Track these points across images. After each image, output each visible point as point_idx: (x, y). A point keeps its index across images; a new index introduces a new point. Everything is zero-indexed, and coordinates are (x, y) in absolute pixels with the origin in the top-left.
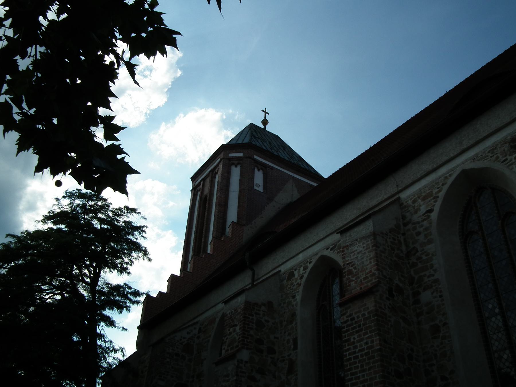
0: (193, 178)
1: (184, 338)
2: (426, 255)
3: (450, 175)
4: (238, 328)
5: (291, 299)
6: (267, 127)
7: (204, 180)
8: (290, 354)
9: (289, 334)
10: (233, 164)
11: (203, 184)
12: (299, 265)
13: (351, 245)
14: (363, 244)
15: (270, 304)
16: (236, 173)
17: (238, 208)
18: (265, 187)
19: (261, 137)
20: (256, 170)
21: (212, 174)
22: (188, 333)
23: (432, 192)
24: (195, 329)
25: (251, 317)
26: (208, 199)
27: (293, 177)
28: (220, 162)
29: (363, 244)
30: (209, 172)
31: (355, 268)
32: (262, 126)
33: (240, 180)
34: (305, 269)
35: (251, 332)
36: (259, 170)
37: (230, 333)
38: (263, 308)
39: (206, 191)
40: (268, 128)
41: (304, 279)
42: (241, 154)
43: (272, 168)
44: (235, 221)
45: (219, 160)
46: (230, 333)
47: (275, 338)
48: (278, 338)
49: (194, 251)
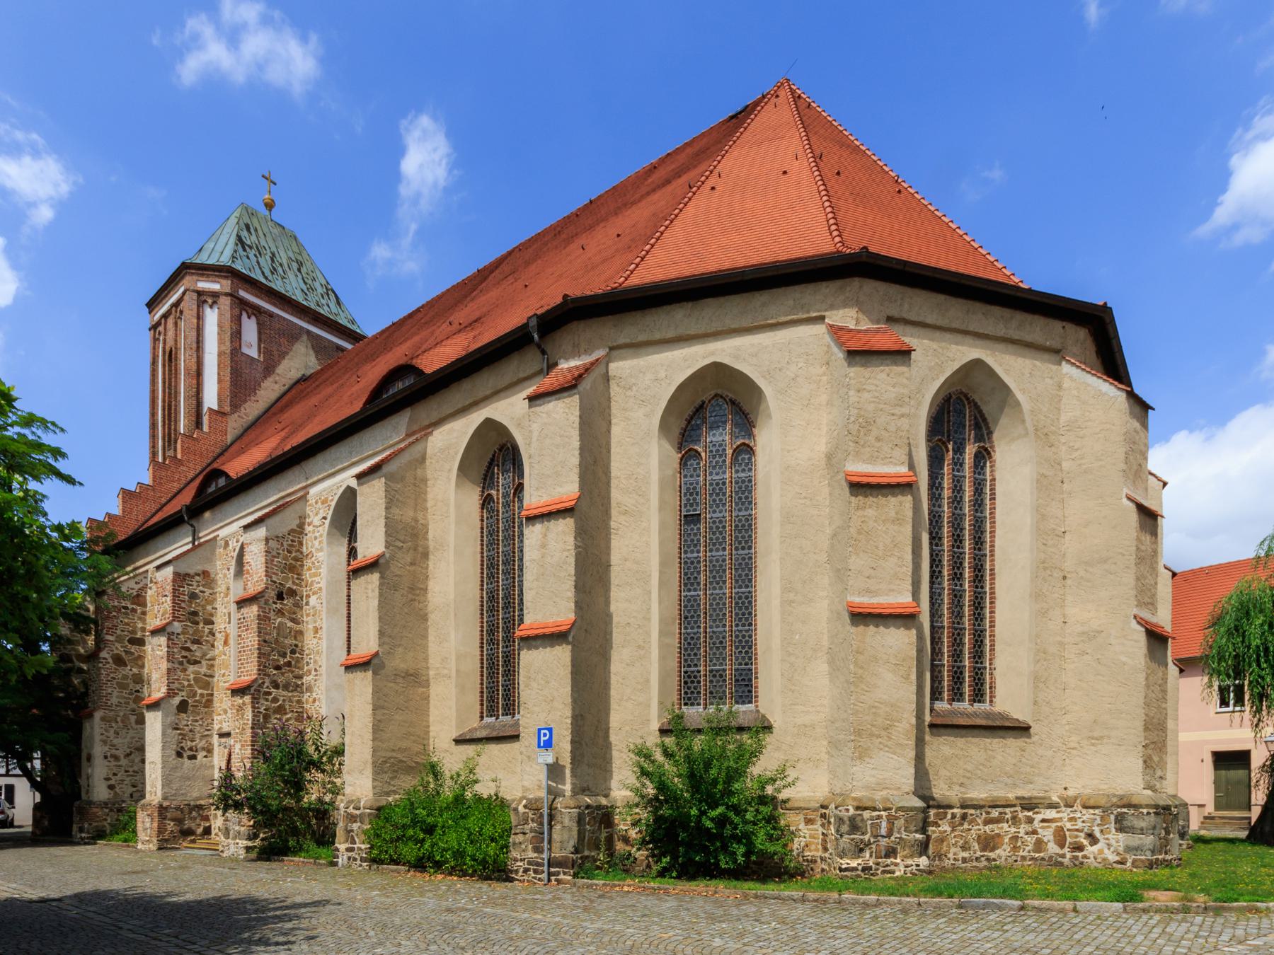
4: (168, 599)
16: (212, 318)
20: (244, 315)
27: (308, 332)
28: (184, 293)
36: (249, 317)
38: (197, 578)
39: (170, 343)
43: (271, 315)
45: (182, 290)
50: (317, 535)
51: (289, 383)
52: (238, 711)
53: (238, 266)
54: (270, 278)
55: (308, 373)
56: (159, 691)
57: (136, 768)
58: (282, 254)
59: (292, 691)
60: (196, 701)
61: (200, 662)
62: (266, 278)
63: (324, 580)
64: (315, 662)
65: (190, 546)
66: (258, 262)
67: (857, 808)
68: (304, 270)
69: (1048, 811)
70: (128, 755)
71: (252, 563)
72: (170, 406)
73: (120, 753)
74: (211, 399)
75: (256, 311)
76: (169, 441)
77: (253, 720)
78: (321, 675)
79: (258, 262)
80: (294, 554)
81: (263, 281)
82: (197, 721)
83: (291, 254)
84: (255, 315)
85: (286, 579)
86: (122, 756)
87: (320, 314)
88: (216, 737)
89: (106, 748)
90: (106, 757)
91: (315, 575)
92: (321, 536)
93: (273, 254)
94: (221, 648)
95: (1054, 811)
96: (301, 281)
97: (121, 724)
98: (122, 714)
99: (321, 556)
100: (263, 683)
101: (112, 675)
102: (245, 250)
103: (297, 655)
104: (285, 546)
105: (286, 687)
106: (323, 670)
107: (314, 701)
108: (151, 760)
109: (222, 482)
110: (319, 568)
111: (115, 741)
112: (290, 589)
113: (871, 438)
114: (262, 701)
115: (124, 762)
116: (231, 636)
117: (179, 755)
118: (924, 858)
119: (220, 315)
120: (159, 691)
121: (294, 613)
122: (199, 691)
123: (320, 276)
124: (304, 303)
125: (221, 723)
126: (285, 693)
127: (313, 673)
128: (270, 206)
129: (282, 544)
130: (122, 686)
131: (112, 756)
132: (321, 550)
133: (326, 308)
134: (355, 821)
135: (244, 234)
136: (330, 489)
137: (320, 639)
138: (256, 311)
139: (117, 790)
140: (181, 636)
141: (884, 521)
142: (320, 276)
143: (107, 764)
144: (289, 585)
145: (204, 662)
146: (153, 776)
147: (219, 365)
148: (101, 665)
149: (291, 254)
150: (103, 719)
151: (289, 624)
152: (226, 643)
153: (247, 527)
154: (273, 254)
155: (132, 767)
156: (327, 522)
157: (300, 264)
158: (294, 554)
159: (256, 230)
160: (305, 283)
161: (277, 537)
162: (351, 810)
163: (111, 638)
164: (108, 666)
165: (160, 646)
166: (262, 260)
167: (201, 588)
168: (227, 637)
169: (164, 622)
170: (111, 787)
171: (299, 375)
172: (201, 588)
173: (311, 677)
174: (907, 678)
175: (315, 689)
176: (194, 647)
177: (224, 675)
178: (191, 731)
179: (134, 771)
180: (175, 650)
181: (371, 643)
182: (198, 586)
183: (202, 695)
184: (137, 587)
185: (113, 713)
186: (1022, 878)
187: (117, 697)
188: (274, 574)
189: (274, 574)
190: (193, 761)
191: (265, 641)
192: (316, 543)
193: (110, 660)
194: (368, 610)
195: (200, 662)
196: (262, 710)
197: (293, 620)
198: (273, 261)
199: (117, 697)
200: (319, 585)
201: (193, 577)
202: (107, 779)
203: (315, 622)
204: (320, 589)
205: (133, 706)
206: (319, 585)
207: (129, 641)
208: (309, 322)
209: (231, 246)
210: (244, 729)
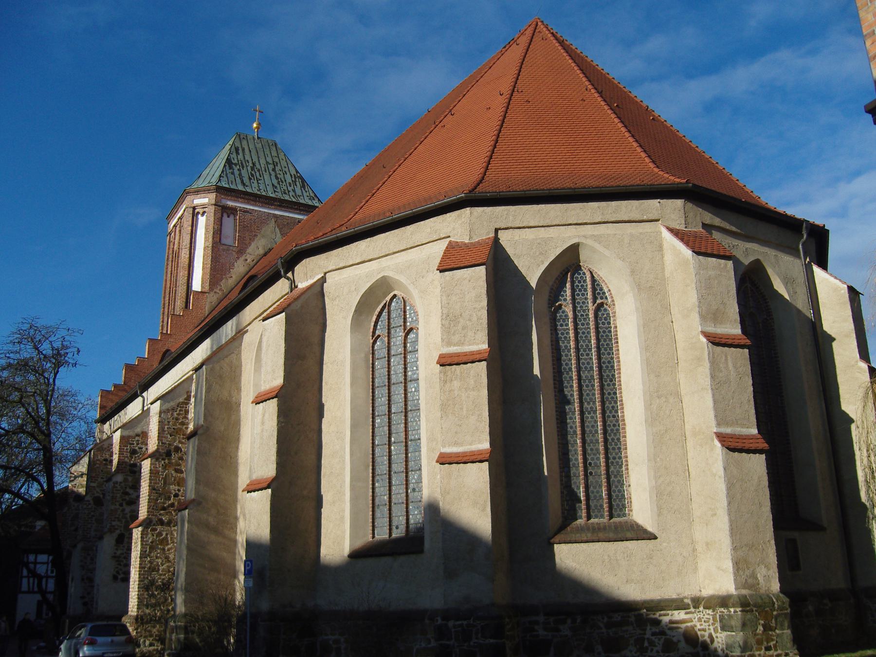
20: (225, 215)
27: (275, 216)
36: (228, 217)
54: (248, 183)
62: (244, 184)
66: (240, 175)
67: (443, 619)
69: (676, 612)
74: (197, 286)
77: (141, 551)
79: (240, 175)
83: (269, 160)
90: (83, 580)
95: (683, 612)
96: (273, 177)
101: (92, 514)
102: (231, 168)
113: (460, 327)
114: (150, 536)
119: (207, 220)
141: (466, 389)
142: (291, 168)
154: (254, 164)
160: (277, 178)
164: (90, 506)
174: (484, 510)
180: (118, 495)
182: (138, 444)
193: (92, 502)
197: (177, 471)
198: (252, 169)
202: (83, 597)
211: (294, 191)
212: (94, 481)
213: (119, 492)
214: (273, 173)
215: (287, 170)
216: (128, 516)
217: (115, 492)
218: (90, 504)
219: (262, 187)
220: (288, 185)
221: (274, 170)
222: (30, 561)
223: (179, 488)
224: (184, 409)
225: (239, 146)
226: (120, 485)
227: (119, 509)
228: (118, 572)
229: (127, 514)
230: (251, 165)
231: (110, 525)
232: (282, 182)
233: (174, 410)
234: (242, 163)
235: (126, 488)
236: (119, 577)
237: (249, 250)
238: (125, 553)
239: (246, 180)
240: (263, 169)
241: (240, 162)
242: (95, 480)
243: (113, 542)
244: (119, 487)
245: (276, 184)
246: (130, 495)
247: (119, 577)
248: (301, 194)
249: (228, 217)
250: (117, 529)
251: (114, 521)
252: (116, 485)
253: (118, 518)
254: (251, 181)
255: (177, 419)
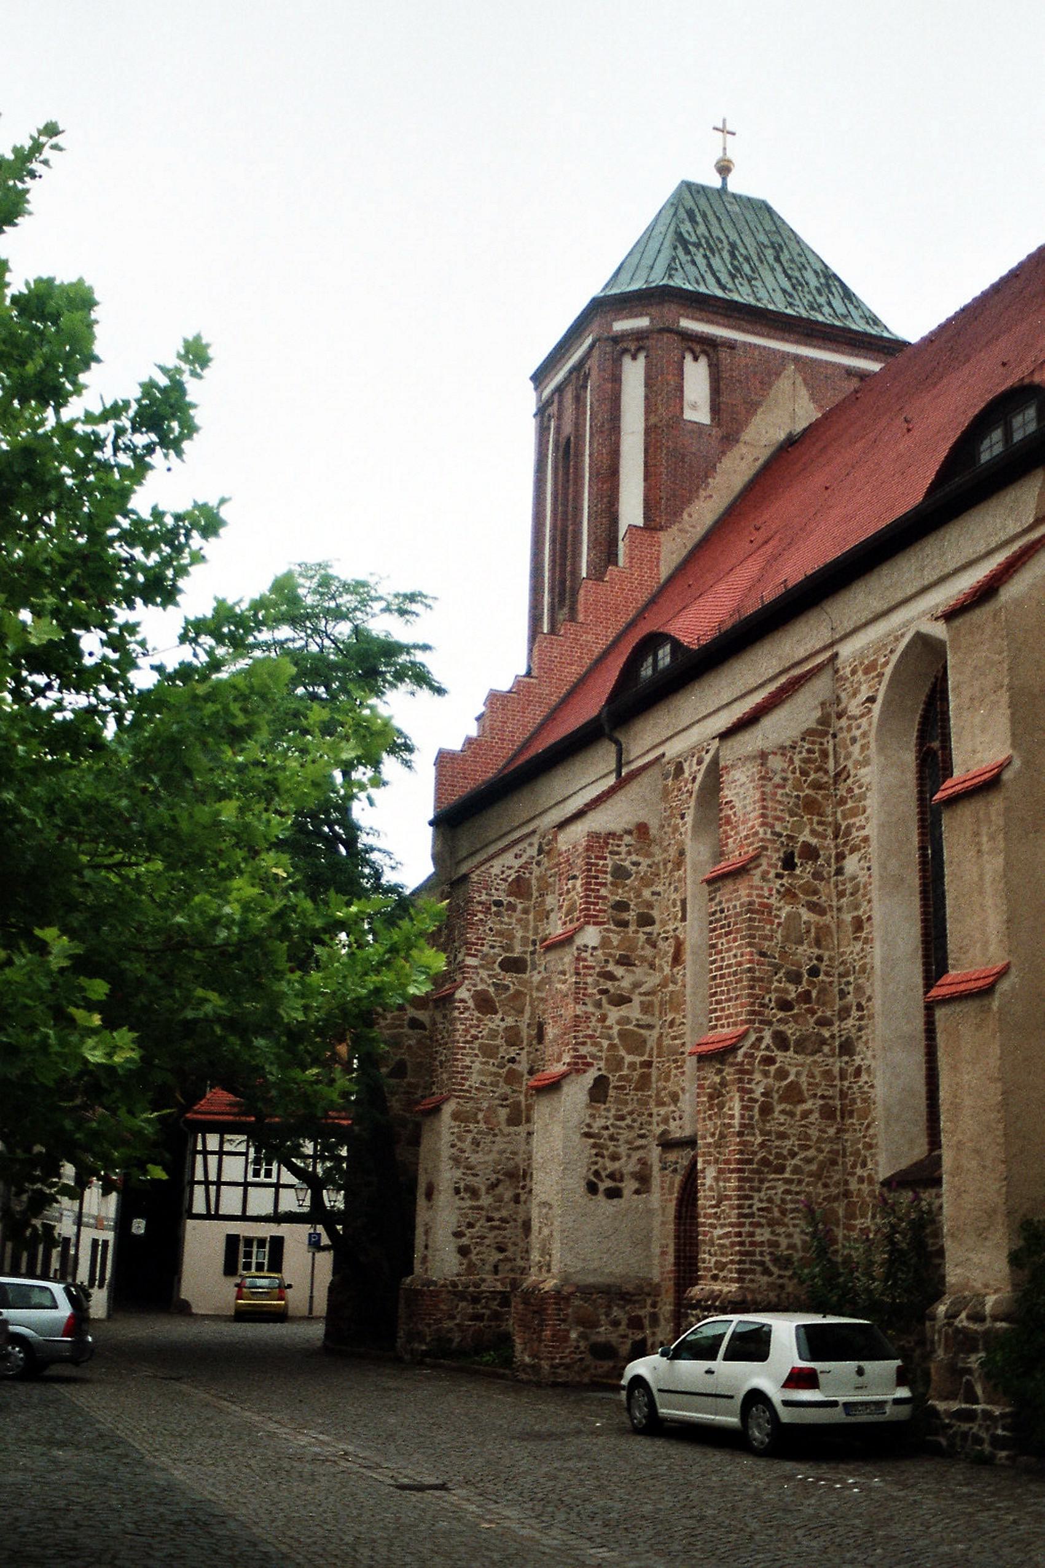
0: (539, 378)
1: (510, 868)
2: (860, 787)
3: (902, 635)
4: (579, 882)
5: (679, 821)
6: (730, 179)
7: (559, 389)
8: (677, 929)
9: (676, 890)
10: (625, 351)
11: (560, 402)
12: (692, 752)
13: (732, 766)
14: (748, 770)
15: (642, 829)
16: (634, 373)
17: (646, 480)
18: (715, 409)
19: (707, 234)
20: (689, 358)
21: (578, 378)
22: (516, 856)
23: (876, 660)
24: (531, 845)
25: (601, 862)
26: (572, 445)
27: (797, 358)
28: (592, 347)
29: (748, 770)
30: (570, 372)
31: (735, 815)
32: (715, 182)
33: (647, 398)
34: (699, 763)
35: (603, 892)
36: (696, 359)
37: (568, 892)
38: (627, 839)
39: (568, 429)
40: (737, 185)
41: (697, 785)
42: (643, 322)
43: (731, 345)
44: (640, 522)
45: (589, 341)
46: (568, 892)
47: (654, 893)
48: (659, 894)
49: (552, 590)
50: (857, 733)
51: (764, 455)
52: (711, 1097)
53: (678, 282)
54: (730, 286)
55: (801, 426)
56: (559, 1060)
57: (504, 1213)
58: (748, 240)
59: (813, 1054)
60: (621, 1078)
61: (630, 1001)
62: (723, 288)
63: (874, 822)
64: (859, 989)
65: (612, 780)
66: (709, 266)
68: (785, 256)
70: (493, 1186)
71: (738, 804)
72: (564, 533)
73: (480, 1183)
75: (707, 346)
76: (562, 594)
78: (871, 1017)
79: (709, 266)
80: (813, 776)
81: (719, 293)
82: (622, 1118)
83: (762, 238)
84: (708, 355)
85: (799, 827)
86: (483, 1189)
87: (817, 322)
88: (656, 1151)
89: (458, 1173)
90: (457, 1191)
91: (854, 812)
92: (864, 735)
93: (733, 246)
94: (667, 970)
97: (483, 1126)
98: (485, 1105)
99: (867, 774)
100: (760, 1039)
101: (473, 1032)
102: (688, 252)
103: (822, 977)
104: (797, 763)
105: (801, 1046)
106: (877, 1005)
107: (858, 1072)
108: (543, 1197)
109: (664, 656)
110: (863, 797)
111: (474, 1159)
112: (806, 845)
114: (757, 1076)
115: (486, 1200)
116: (688, 947)
117: (592, 1188)
118: (443, 957)
120: (559, 1060)
121: (815, 892)
122: (629, 1059)
123: (812, 259)
124: (789, 311)
125: (666, 1121)
126: (800, 1058)
127: (855, 1013)
128: (724, 169)
129: (791, 761)
130: (489, 1052)
131: (468, 1188)
132: (866, 762)
133: (826, 310)
134: (975, 1350)
135: (686, 227)
136: (880, 646)
137: (866, 941)
138: (707, 346)
139: (473, 1257)
140: (599, 952)
143: (459, 1203)
144: (805, 837)
145: (637, 999)
146: (546, 1231)
147: (646, 450)
148: (456, 1013)
149: (762, 238)
150: (456, 1116)
151: (806, 915)
152: (677, 960)
153: (725, 735)
154: (733, 246)
155: (498, 1209)
156: (876, 708)
157: (778, 249)
158: (813, 776)
159: (704, 216)
160: (789, 278)
161: (783, 748)
162: (962, 1321)
163: (471, 961)
165: (563, 973)
166: (716, 262)
167: (634, 858)
168: (679, 946)
169: (570, 927)
170: (463, 1251)
171: (782, 436)
172: (634, 858)
173: (850, 1022)
175: (860, 1047)
176: (619, 971)
177: (672, 1024)
178: (612, 1138)
179: (503, 1220)
180: (589, 980)
181: (992, 948)
182: (629, 853)
183: (632, 1066)
184: (517, 863)
185: (471, 1104)
186: (665, 986)
187: (481, 1073)
188: (778, 818)
189: (778, 818)
190: (615, 1201)
191: (763, 954)
192: (856, 749)
193: (471, 1003)
194: (981, 877)
195: (630, 1001)
196: (756, 1095)
198: (733, 256)
199: (481, 1073)
200: (863, 833)
201: (620, 838)
202: (458, 1235)
203: (857, 907)
204: (866, 839)
205: (505, 1089)
206: (863, 833)
207: (502, 965)
208: (797, 342)
209: (666, 253)
210: (722, 1136)
211: (830, 304)
212: (473, 952)
213: (591, 971)
214: (776, 265)
215: (803, 260)
216: (615, 1031)
217: (582, 971)
218: (467, 1009)
219: (762, 293)
220: (814, 292)
221: (777, 259)
222: (209, 1149)
223: (820, 952)
224: (817, 747)
225: (694, 207)
226: (592, 955)
227: (593, 1014)
228: (597, 1173)
229: (610, 1028)
230: (727, 247)
231: (572, 1053)
232: (801, 285)
233: (795, 748)
234: (707, 242)
235: (607, 961)
236: (602, 1186)
237: (748, 435)
238: (612, 1125)
239: (725, 278)
240: (755, 258)
241: (703, 241)
242: (476, 950)
243: (583, 1097)
244: (590, 959)
245: (789, 289)
246: (617, 979)
247: (602, 1186)
248: (844, 311)
249: (696, 359)
250: (590, 1065)
251: (584, 1044)
252: (584, 954)
253: (591, 1037)
254: (736, 281)
255: (805, 773)
